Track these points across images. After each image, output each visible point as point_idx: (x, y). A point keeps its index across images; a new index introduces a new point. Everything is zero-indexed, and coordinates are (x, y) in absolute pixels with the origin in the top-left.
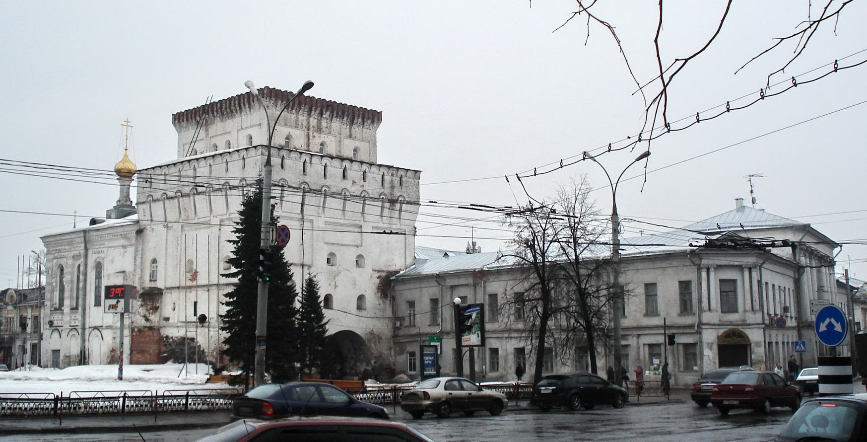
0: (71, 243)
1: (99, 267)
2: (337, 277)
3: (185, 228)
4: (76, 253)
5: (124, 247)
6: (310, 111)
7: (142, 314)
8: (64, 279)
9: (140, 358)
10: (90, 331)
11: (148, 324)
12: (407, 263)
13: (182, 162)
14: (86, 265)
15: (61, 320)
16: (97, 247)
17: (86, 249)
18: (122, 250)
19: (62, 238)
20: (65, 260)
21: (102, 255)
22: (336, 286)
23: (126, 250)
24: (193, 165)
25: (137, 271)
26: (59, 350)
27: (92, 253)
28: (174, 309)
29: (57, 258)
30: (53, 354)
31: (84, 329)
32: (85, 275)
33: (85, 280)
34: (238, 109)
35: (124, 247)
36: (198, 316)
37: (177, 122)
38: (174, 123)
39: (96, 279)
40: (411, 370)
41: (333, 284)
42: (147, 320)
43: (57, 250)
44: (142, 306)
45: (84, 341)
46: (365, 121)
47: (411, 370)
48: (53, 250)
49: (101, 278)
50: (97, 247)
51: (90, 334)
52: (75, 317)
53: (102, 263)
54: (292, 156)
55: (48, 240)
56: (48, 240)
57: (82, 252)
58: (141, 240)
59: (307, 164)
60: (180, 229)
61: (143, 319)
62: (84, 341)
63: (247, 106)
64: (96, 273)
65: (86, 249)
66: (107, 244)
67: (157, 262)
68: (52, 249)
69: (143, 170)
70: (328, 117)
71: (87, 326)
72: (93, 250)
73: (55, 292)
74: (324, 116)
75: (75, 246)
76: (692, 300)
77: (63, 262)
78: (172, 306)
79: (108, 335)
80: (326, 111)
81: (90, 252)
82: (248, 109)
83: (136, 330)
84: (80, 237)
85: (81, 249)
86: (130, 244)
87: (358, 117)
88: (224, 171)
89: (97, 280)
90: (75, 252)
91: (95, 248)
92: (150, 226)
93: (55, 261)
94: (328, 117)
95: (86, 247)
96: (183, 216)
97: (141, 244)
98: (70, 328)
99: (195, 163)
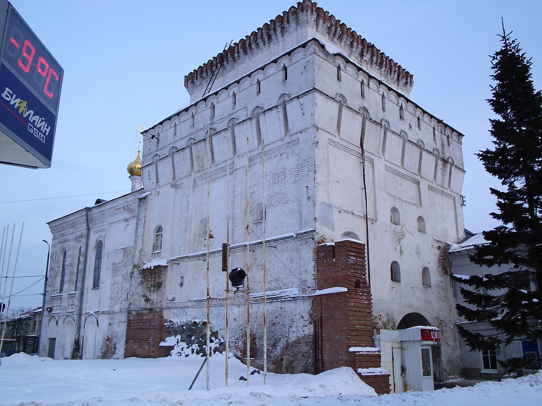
0: (74, 225)
1: (100, 246)
2: (401, 240)
3: (198, 182)
4: (78, 234)
5: (126, 220)
6: (351, 45)
7: (141, 293)
8: (66, 263)
9: (136, 349)
10: (86, 316)
11: (148, 306)
12: (459, 236)
13: (196, 105)
14: (87, 245)
15: (60, 306)
16: (99, 225)
17: (89, 229)
18: (124, 224)
19: (66, 220)
20: (68, 243)
21: (103, 233)
22: (401, 252)
23: (128, 223)
24: (211, 102)
25: (138, 242)
26: (55, 339)
27: (94, 232)
28: (181, 285)
29: (61, 242)
30: (50, 342)
31: (80, 315)
32: (86, 257)
33: (85, 262)
34: (266, 39)
35: (126, 220)
36: (230, 271)
37: (189, 82)
38: (186, 86)
39: (96, 259)
40: (486, 367)
41: (398, 250)
42: (147, 300)
43: (61, 234)
44: (142, 283)
45: (79, 328)
46: (400, 79)
47: (486, 367)
48: (58, 235)
49: (101, 258)
50: (99, 225)
51: (86, 319)
52: (72, 302)
53: (103, 241)
54: (348, 69)
55: (54, 225)
56: (54, 225)
57: (85, 232)
58: (144, 207)
59: (365, 86)
60: (192, 185)
61: (143, 299)
62: (79, 328)
63: (279, 30)
64: (96, 253)
65: (89, 229)
66: (109, 220)
67: (162, 231)
68: (58, 234)
69: (150, 129)
70: (368, 61)
71: (84, 312)
72: (95, 230)
73: (57, 277)
74: (364, 58)
75: (78, 227)
76: (54, 354)
77: (65, 245)
78: (179, 281)
79: (104, 320)
80: (367, 53)
81: (92, 231)
82: (279, 35)
83: (134, 313)
84: (82, 216)
85: (82, 229)
86: (132, 216)
87: (395, 74)
88: (255, 94)
89: (97, 260)
90: (77, 234)
91: (96, 228)
92: (155, 190)
93: (59, 245)
94: (368, 61)
95: (88, 225)
96: (196, 168)
97: (143, 211)
98: (67, 314)
99: (213, 100)
